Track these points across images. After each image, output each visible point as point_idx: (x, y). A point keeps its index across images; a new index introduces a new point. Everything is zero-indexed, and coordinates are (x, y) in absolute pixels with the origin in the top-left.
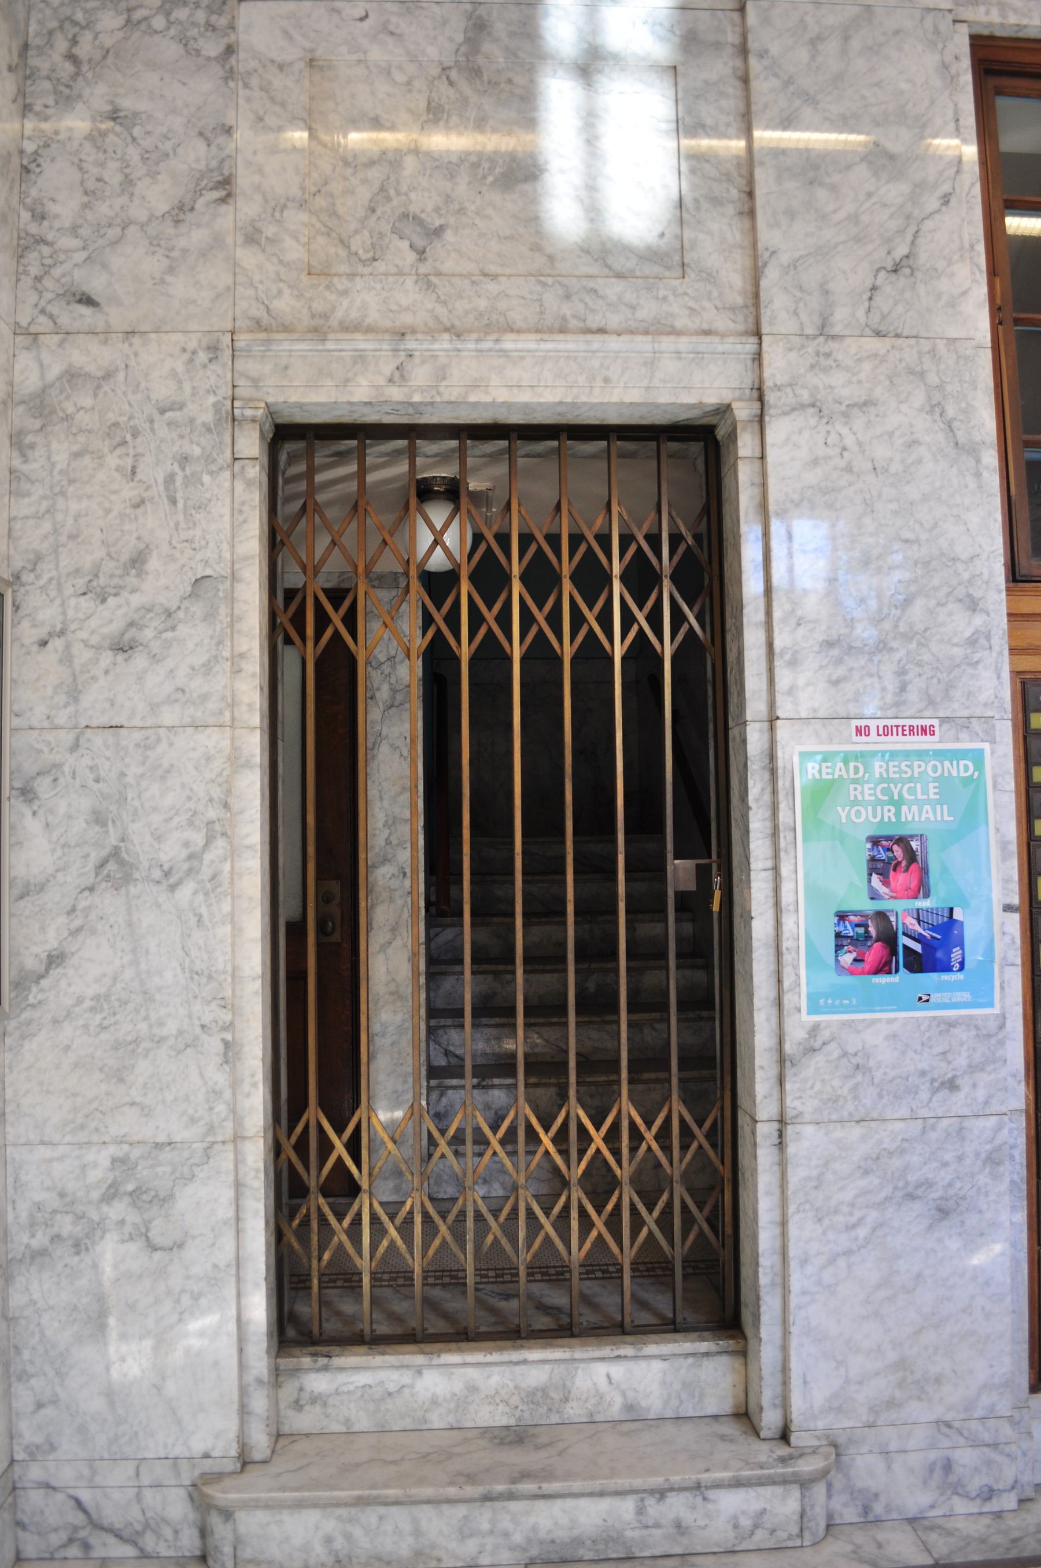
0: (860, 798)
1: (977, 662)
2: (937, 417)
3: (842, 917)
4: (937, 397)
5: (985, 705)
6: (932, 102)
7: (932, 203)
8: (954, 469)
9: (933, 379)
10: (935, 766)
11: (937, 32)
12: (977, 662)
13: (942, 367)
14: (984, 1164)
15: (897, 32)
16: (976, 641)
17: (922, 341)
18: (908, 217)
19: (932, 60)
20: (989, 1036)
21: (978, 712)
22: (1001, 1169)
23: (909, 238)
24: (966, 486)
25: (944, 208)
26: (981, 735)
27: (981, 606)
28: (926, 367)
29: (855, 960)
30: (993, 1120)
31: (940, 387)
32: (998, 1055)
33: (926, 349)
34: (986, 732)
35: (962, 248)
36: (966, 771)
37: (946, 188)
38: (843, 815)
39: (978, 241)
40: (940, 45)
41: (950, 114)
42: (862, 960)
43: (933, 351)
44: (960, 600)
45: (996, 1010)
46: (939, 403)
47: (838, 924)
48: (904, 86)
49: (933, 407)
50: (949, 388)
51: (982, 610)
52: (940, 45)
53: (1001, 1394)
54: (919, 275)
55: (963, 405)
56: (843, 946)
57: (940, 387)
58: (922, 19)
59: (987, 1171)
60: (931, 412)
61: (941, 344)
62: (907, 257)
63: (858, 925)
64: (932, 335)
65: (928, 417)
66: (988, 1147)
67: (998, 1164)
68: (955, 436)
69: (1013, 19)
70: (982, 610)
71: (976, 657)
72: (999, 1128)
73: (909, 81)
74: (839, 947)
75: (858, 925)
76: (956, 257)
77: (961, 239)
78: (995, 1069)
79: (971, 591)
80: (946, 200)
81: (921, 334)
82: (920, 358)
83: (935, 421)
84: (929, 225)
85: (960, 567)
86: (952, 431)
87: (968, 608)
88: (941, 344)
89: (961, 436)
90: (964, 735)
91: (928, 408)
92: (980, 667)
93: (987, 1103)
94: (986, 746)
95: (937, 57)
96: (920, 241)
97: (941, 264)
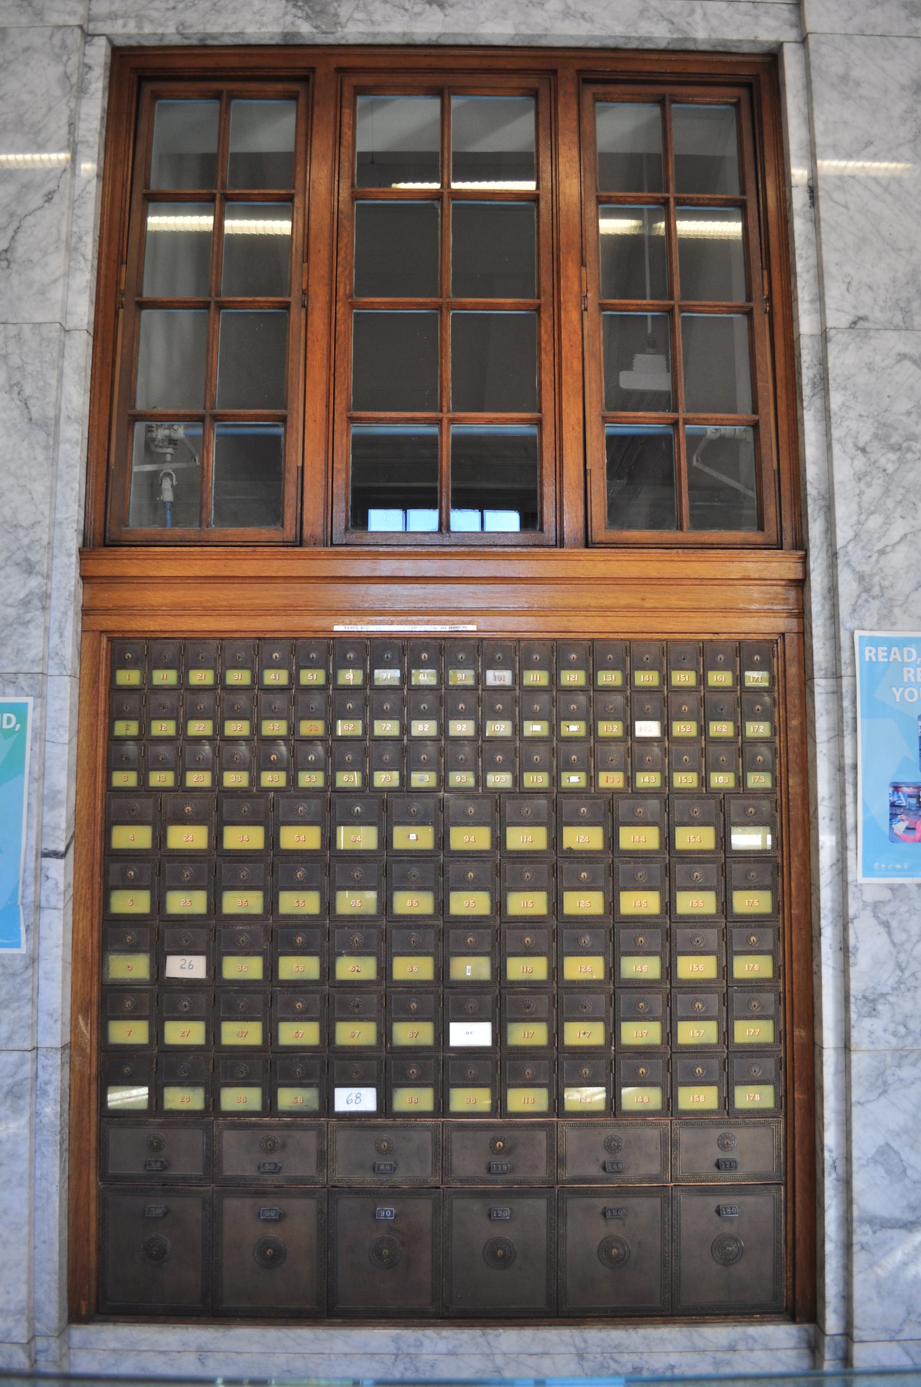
0: (913, 680)
1: (29, 622)
2: (15, 395)
3: (896, 788)
4: (17, 377)
5: (33, 661)
6: (50, 109)
7: (36, 200)
8: (26, 444)
9: (15, 360)
10: (909, 657)
11: (64, 46)
12: (29, 622)
13: (25, 349)
14: (6, 1097)
15: (26, 50)
16: (29, 602)
17: (10, 326)
18: (12, 215)
19: (54, 72)
20: (14, 975)
21: (25, 668)
22: (22, 1103)
23: (10, 232)
24: (35, 458)
25: (47, 205)
26: (26, 689)
27: (37, 568)
28: (9, 350)
29: (907, 828)
30: (15, 1056)
31: (21, 368)
32: (22, 993)
33: (12, 334)
34: (31, 687)
35: (59, 239)
36: (9, 723)
37: (51, 186)
38: (898, 695)
39: (87, 233)
40: (65, 58)
41: (65, 119)
42: (914, 829)
43: (18, 337)
44: (18, 564)
45: (23, 950)
46: (19, 383)
47: (893, 794)
48: (25, 97)
49: (11, 387)
50: (29, 369)
51: (38, 573)
52: (65, 58)
53: (17, 1321)
54: (14, 266)
55: (41, 384)
56: (896, 815)
57: (21, 368)
58: (52, 35)
59: (8, 1103)
60: (9, 392)
61: (27, 329)
62: (6, 251)
63: (910, 796)
64: (20, 321)
65: (7, 396)
66: (10, 1081)
67: (19, 1098)
68: (29, 412)
69: (148, 29)
70: (38, 573)
71: (28, 617)
72: (21, 1063)
73: (31, 92)
74: (893, 816)
75: (910, 796)
76: (52, 249)
77: (59, 231)
78: (19, 1007)
79: (29, 556)
80: (49, 197)
81: (10, 320)
82: (5, 342)
83: (13, 399)
84: (31, 220)
85: (21, 533)
86: (27, 407)
87: (25, 571)
88: (27, 329)
89: (35, 413)
90: (10, 690)
91: (7, 388)
92: (30, 626)
93: (10, 1038)
94: (30, 701)
95: (61, 69)
96: (21, 236)
97: (36, 256)
